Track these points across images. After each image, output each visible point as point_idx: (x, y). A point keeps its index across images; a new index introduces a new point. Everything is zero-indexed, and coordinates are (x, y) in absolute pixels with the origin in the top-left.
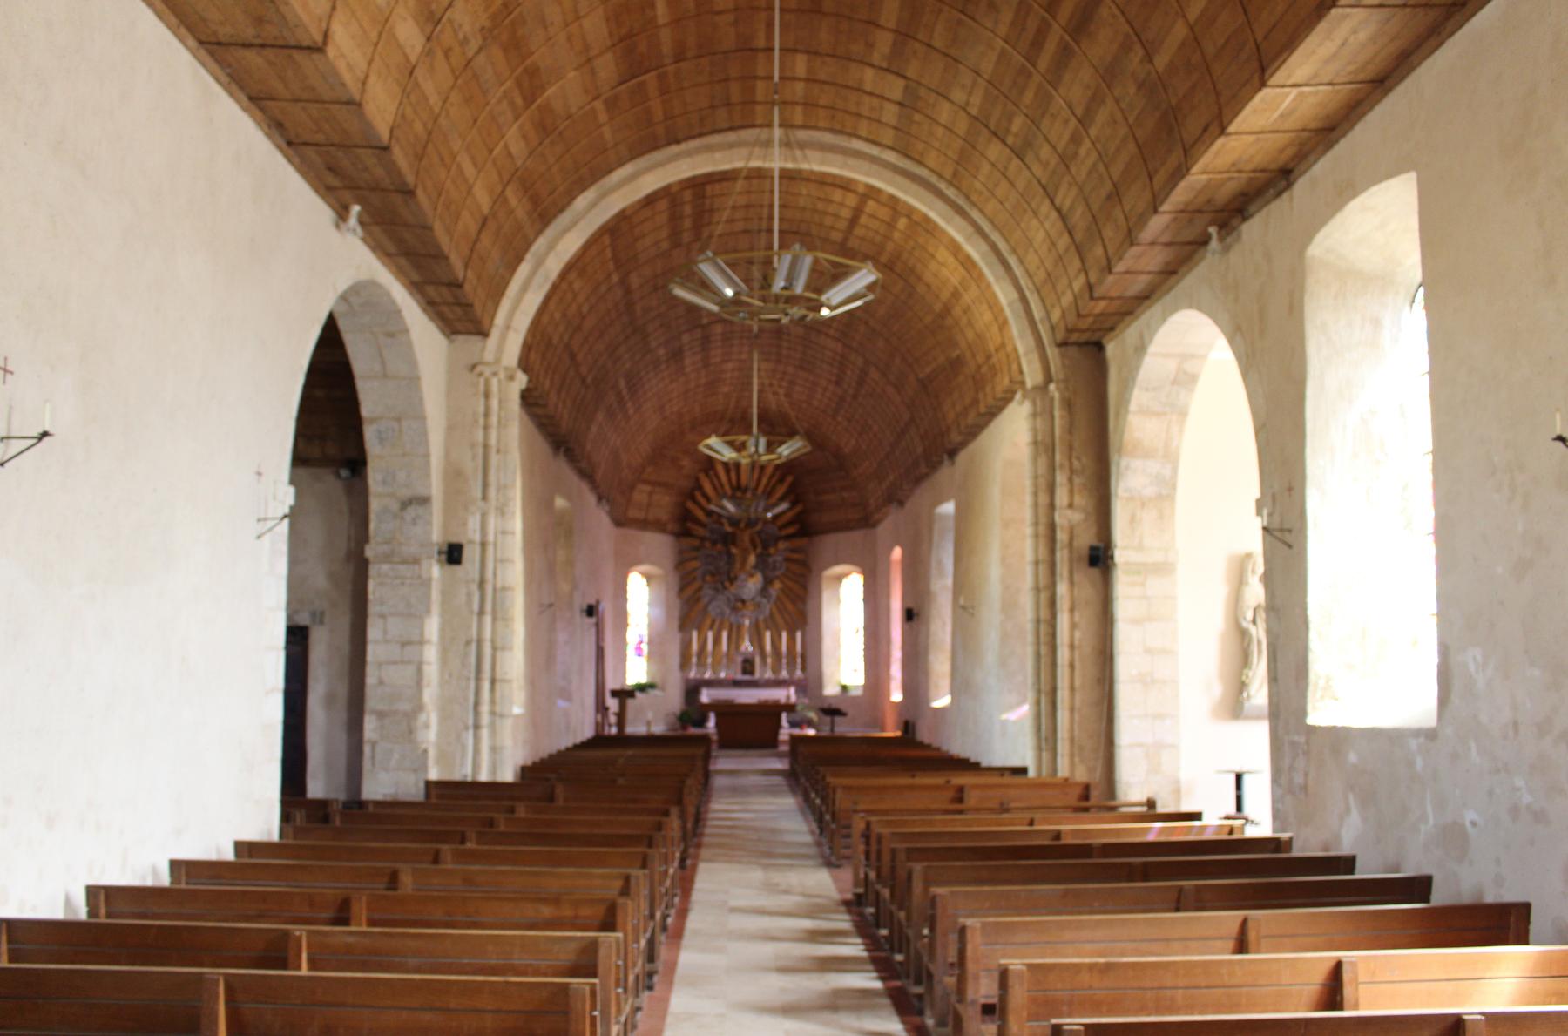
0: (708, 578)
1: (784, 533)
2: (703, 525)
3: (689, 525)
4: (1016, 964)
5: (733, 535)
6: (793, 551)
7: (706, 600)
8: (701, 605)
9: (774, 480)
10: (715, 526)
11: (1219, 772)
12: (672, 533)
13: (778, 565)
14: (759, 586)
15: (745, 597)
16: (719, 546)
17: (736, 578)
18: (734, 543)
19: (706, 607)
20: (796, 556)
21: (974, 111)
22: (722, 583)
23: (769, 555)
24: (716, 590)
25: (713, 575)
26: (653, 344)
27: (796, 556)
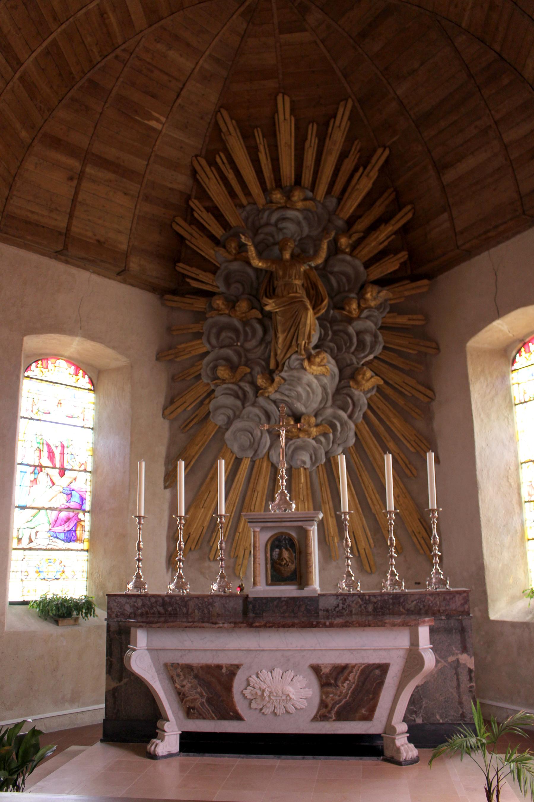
0: (223, 372)
1: (377, 272)
2: (214, 270)
3: (181, 267)
4: (359, 264)
5: (271, 276)
6: (395, 309)
7: (220, 419)
8: (210, 430)
9: (348, 165)
10: (235, 266)
11: (67, 416)
12: (153, 289)
13: (368, 339)
14: (331, 385)
15: (300, 407)
16: (243, 305)
17: (280, 367)
18: (271, 293)
19: (222, 431)
20: (402, 320)
21: (493, 749)
22: (253, 383)
23: (350, 320)
24: (243, 399)
25: (233, 368)
26: (295, 199)
27: (402, 320)
